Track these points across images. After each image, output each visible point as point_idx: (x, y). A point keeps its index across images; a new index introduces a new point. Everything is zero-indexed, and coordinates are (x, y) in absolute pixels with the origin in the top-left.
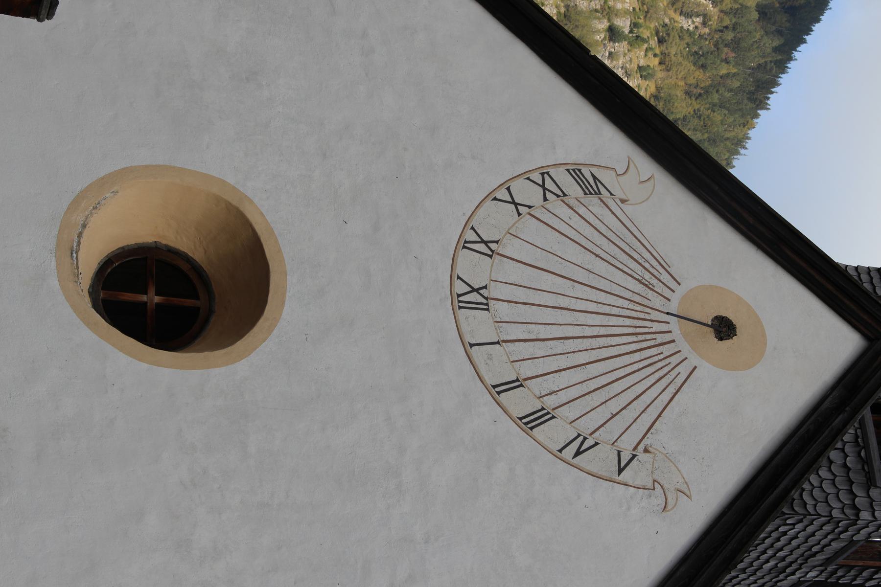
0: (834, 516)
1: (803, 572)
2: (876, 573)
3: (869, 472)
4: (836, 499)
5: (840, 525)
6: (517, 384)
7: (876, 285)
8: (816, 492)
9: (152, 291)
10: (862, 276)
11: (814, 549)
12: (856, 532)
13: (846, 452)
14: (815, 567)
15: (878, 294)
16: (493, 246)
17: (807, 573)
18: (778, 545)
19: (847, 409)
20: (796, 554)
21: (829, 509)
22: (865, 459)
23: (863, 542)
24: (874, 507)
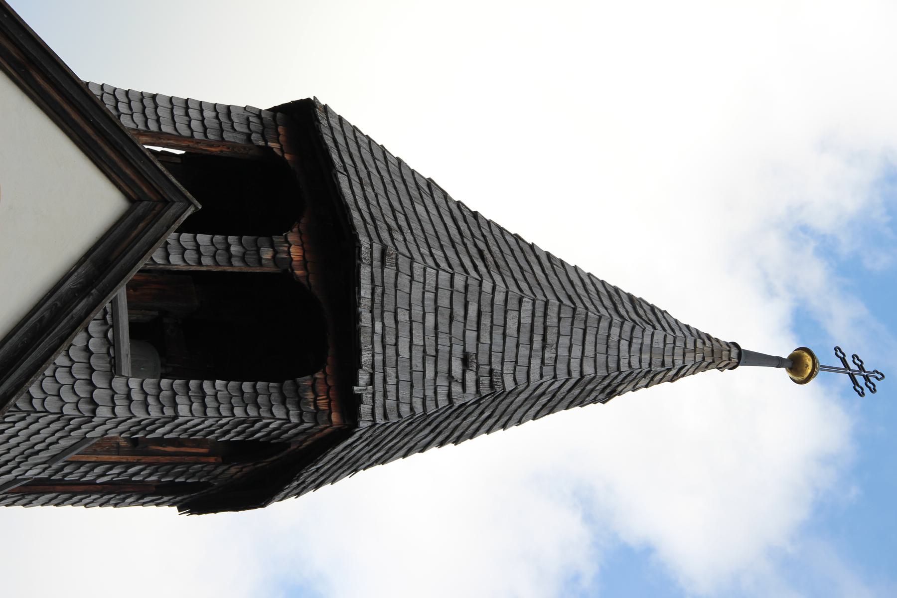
0: (65, 413)
1: (22, 470)
2: (111, 469)
3: (114, 358)
4: (71, 391)
5: (71, 423)
7: (148, 117)
10: (132, 103)
11: (37, 448)
12: (90, 429)
13: (90, 333)
14: (36, 465)
15: (149, 129)
17: (27, 471)
19: (93, 291)
21: (61, 403)
22: (112, 342)
23: (98, 439)
24: (115, 401)
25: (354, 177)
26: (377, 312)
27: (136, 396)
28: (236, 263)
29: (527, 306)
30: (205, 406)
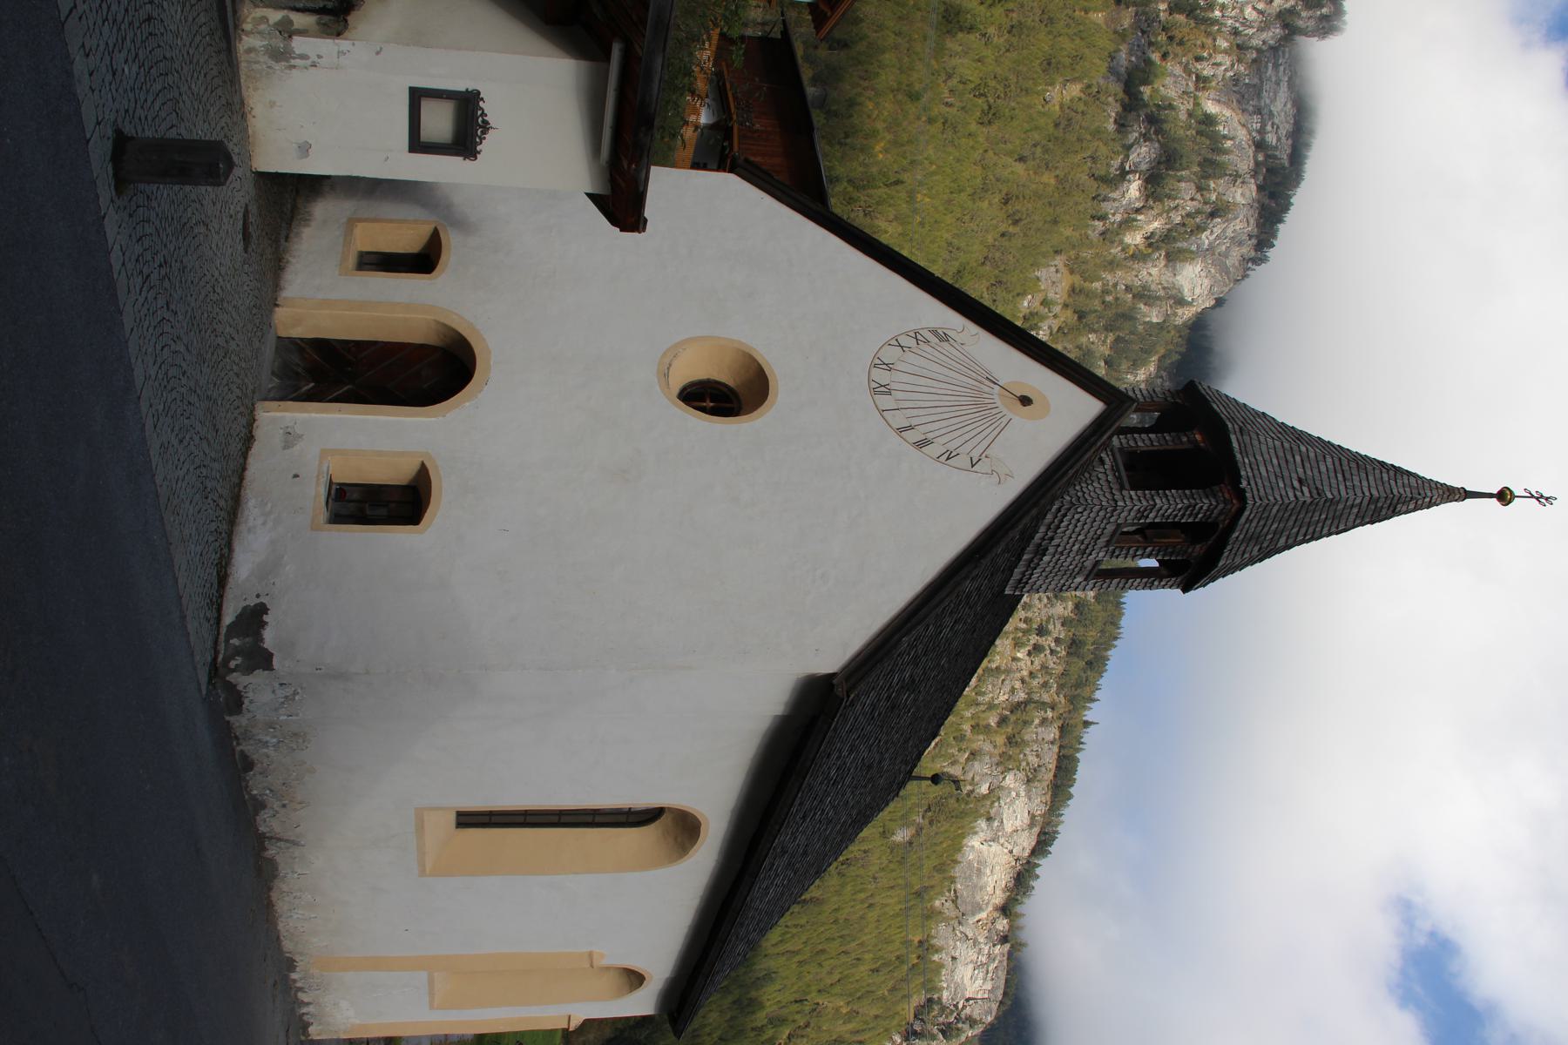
6: (910, 428)
9: (708, 401)
16: (891, 366)
25: (1218, 403)
26: (1244, 455)
27: (1134, 497)
28: (1170, 443)
29: (1329, 460)
30: (1168, 500)
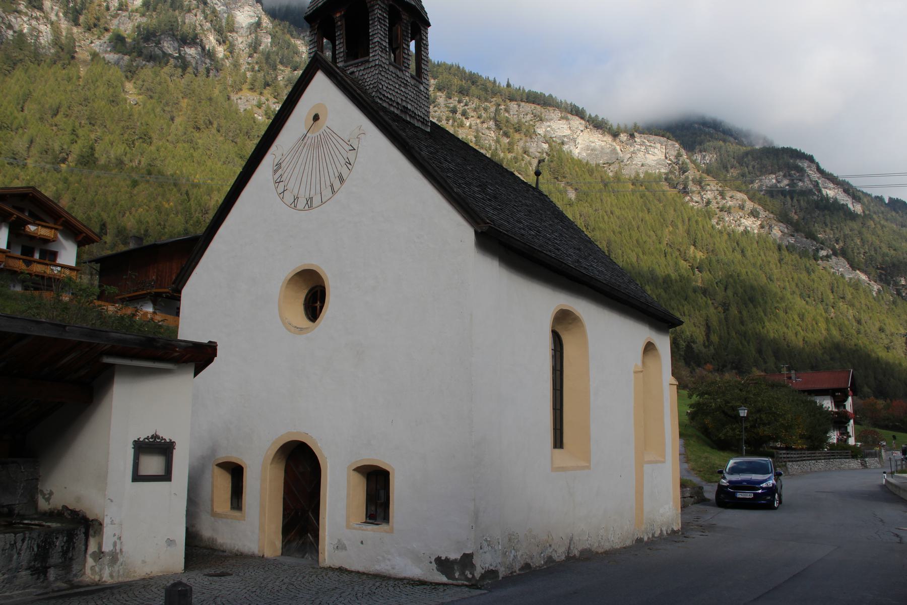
6: (332, 186)
8: (371, 79)
18: (392, 88)
20: (396, 81)
